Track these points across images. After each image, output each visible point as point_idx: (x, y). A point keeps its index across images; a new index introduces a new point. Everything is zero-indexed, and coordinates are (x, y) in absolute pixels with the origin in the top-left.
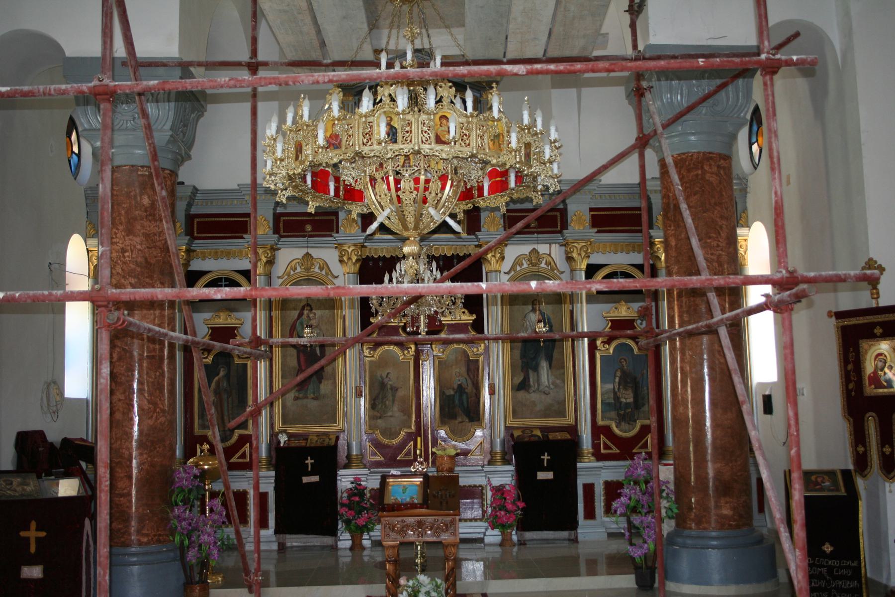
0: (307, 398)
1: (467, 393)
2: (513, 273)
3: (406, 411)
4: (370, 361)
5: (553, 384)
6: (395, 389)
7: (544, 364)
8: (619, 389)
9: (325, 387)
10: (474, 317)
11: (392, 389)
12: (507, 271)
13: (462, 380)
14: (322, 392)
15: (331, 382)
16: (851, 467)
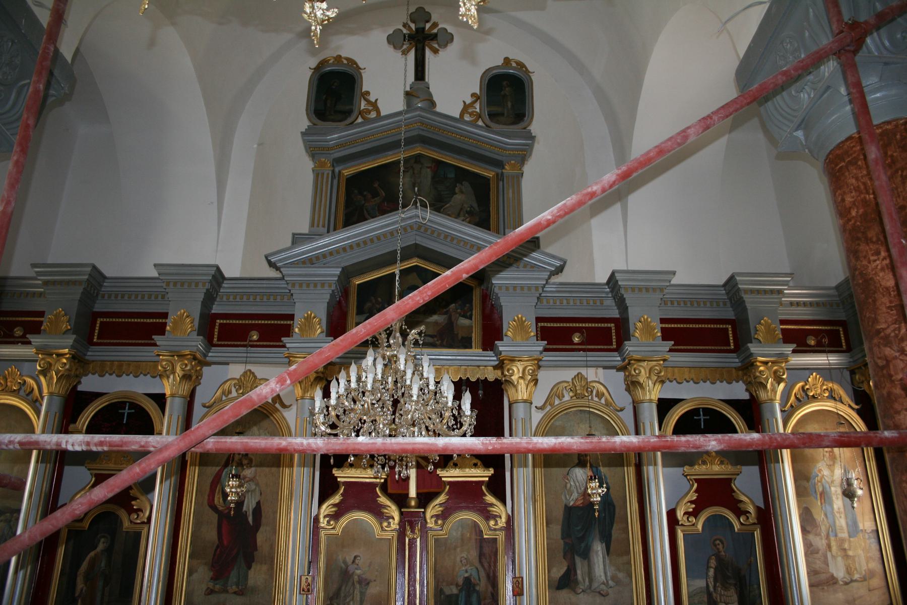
0: (227, 592)
1: (478, 592)
2: (548, 408)
5: (613, 578)
6: (365, 583)
7: (598, 548)
8: (715, 587)
9: (256, 576)
10: (491, 472)
11: (360, 582)
12: (540, 404)
13: (471, 572)
14: (251, 582)
15: (265, 568)
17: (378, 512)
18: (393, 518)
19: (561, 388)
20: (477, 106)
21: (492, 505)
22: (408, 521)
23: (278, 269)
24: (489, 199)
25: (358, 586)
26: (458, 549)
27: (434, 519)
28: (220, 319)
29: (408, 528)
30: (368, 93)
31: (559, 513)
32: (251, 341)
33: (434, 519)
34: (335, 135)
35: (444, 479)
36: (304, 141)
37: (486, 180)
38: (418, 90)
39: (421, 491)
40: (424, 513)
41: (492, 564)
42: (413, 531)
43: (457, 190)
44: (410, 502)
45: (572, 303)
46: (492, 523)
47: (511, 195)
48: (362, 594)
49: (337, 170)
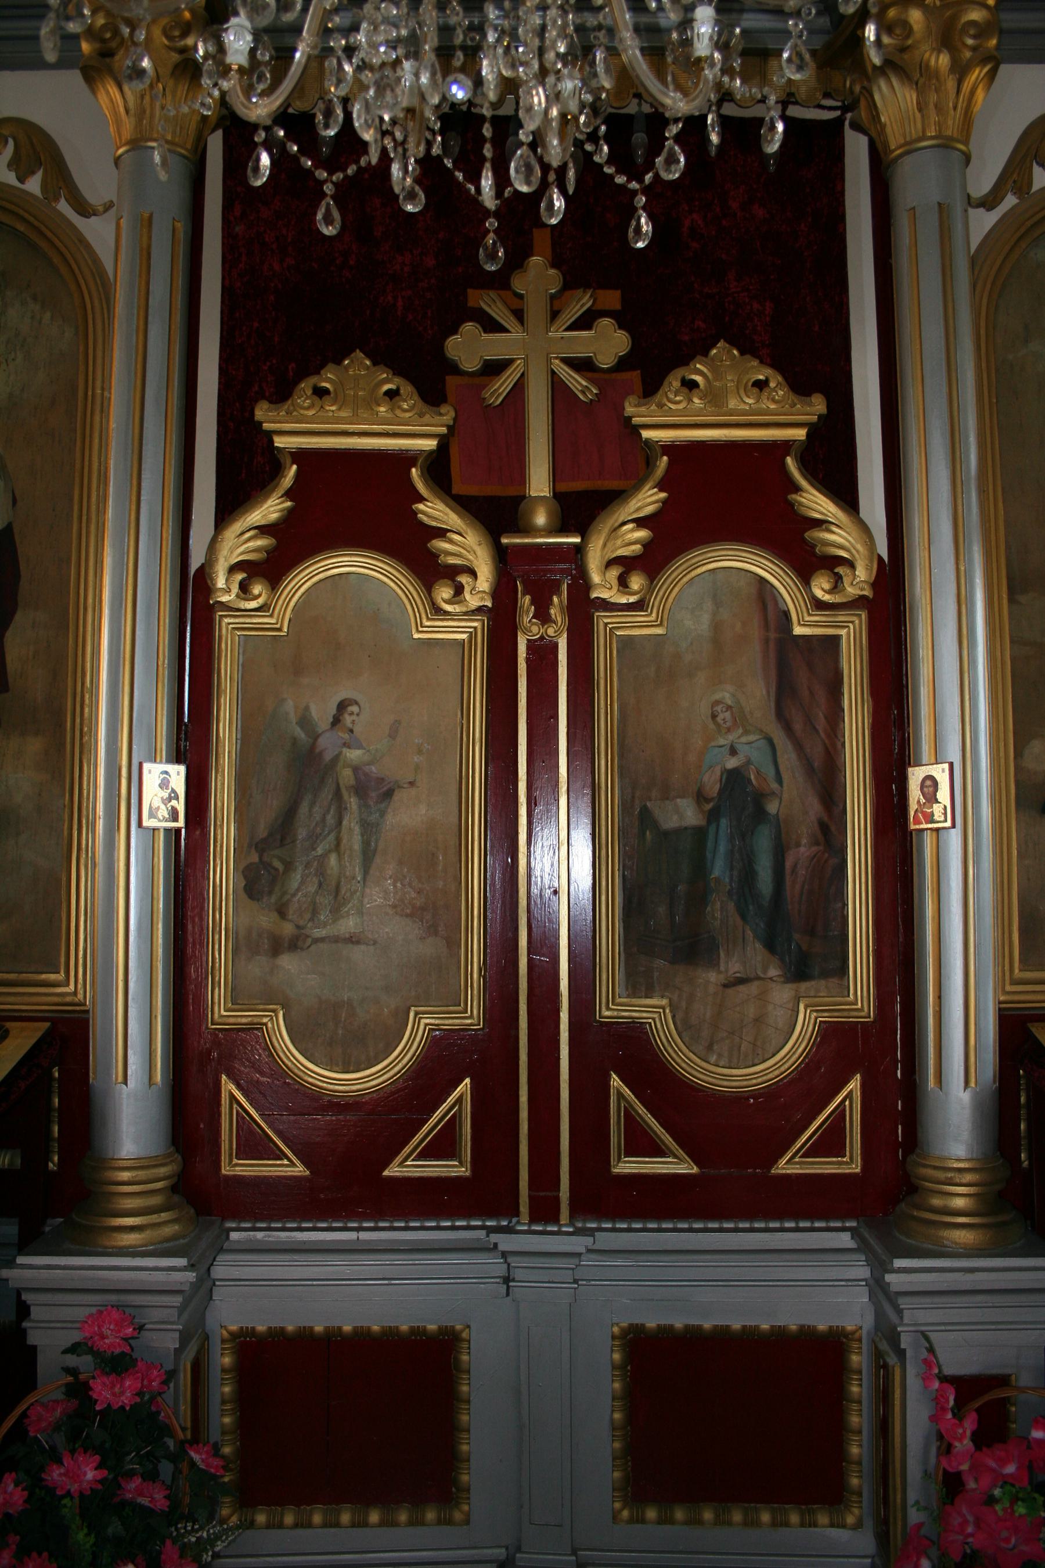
2: (1010, 201)
3: (438, 915)
6: (377, 792)
10: (818, 405)
13: (750, 751)
15: (34, 745)
17: (430, 571)
18: (473, 574)
27: (614, 573)
33: (614, 573)
35: (646, 434)
39: (563, 487)
40: (579, 551)
42: (543, 616)
44: (531, 512)
46: (821, 587)
48: (369, 829)
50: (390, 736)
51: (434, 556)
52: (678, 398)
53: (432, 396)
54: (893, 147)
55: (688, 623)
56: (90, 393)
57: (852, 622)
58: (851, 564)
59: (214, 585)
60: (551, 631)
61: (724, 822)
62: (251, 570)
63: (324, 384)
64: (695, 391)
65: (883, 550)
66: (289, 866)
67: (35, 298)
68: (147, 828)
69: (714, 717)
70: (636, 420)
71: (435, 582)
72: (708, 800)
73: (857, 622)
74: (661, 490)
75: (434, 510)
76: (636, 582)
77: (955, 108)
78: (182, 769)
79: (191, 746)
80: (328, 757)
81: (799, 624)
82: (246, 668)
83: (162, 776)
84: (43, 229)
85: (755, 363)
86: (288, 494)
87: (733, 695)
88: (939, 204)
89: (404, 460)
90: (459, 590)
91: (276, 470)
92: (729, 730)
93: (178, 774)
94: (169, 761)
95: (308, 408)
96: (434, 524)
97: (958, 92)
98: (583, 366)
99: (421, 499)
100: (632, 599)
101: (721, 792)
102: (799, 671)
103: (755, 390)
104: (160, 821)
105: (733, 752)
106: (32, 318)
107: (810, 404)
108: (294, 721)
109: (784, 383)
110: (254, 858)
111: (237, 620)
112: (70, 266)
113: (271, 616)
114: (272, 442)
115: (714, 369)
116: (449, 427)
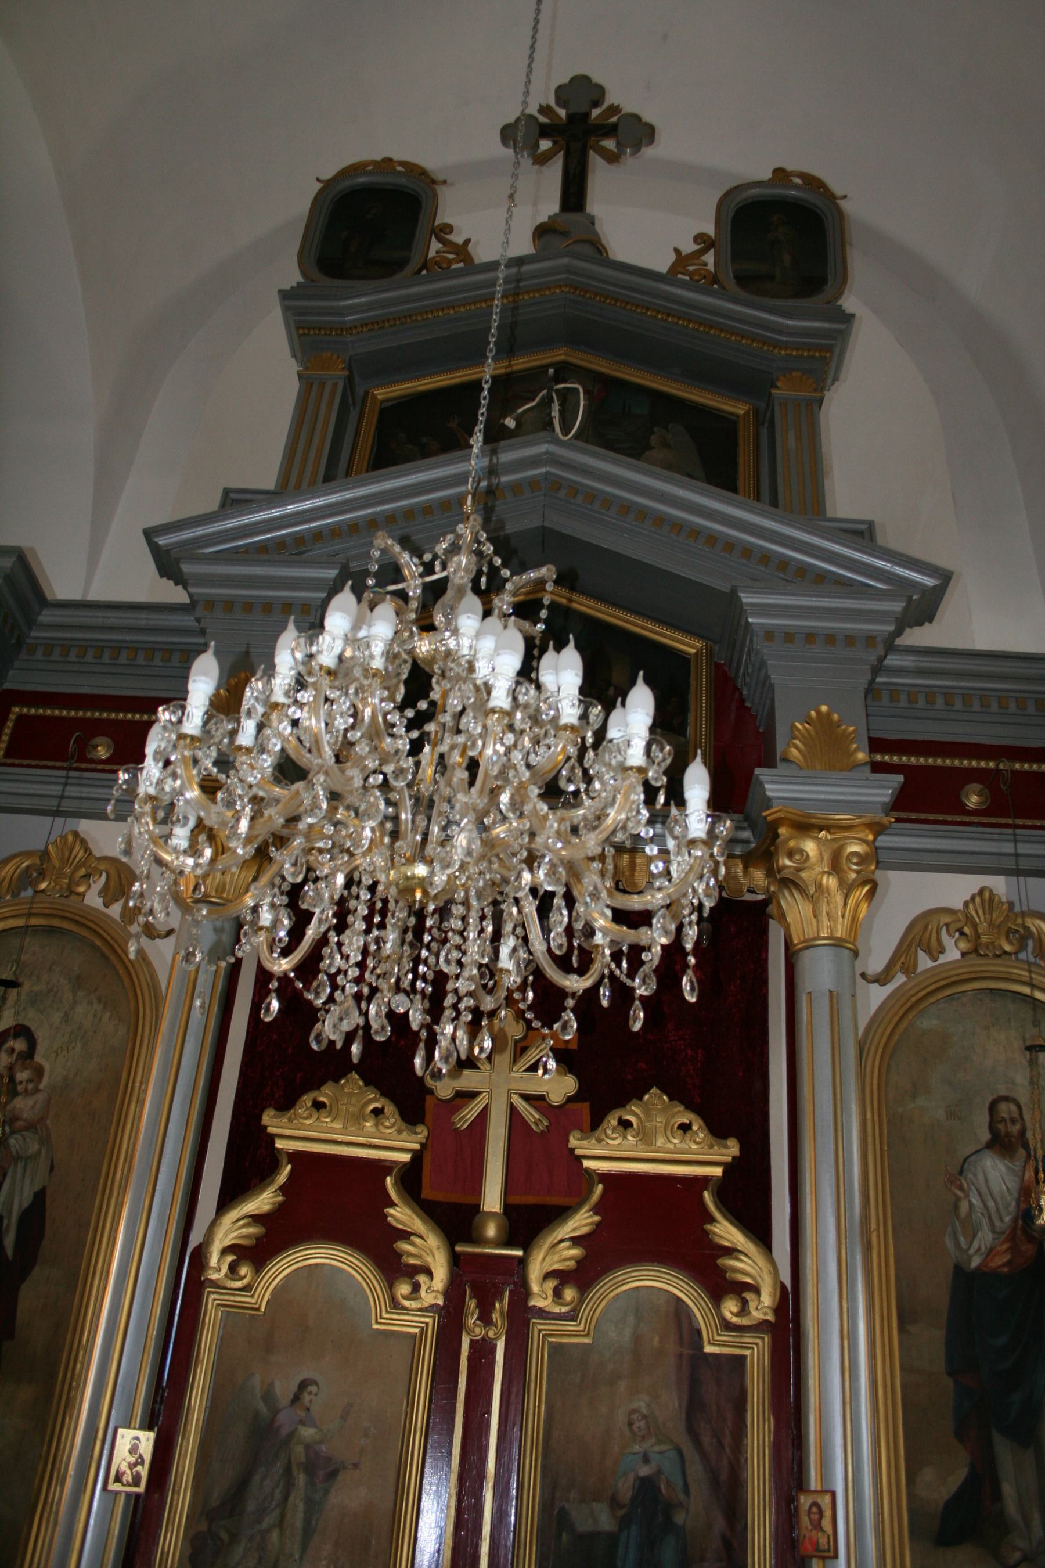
2: (900, 979)
4: (232, 1314)
6: (324, 1470)
10: (732, 1149)
16: (623, 112)
17: (393, 1267)
18: (430, 1274)
19: (932, 927)
20: (709, 258)
21: (731, 1251)
22: (479, 1280)
23: (180, 580)
24: (735, 464)
25: (301, 1479)
26: (622, 1385)
27: (551, 1284)
28: (23, 704)
29: (471, 1304)
30: (448, 228)
31: (937, 1291)
32: (92, 761)
33: (551, 1284)
34: (358, 301)
35: (586, 1164)
36: (286, 309)
37: (728, 425)
38: (570, 227)
39: (515, 1200)
40: (522, 1262)
41: (727, 1440)
42: (485, 1319)
43: (654, 440)
44: (483, 1226)
45: (958, 705)
46: (730, 1308)
47: (792, 442)
48: (312, 1506)
49: (360, 392)
50: (342, 1417)
51: (398, 1255)
52: (614, 1135)
53: (411, 1116)
54: (796, 942)
55: (613, 1335)
56: (130, 1085)
57: (757, 1344)
58: (756, 1290)
59: (208, 1263)
60: (491, 1334)
61: (634, 1529)
62: (239, 1252)
63: (322, 1099)
64: (629, 1130)
65: (786, 1279)
66: (234, 1538)
67: (99, 1000)
68: (111, 1491)
69: (630, 1424)
70: (578, 1152)
71: (397, 1278)
72: (621, 1506)
73: (761, 1344)
74: (596, 1214)
75: (401, 1214)
76: (569, 1294)
77: (843, 916)
78: (152, 1435)
79: (163, 1414)
80: (284, 1432)
81: (710, 1343)
82: (225, 1341)
83: (133, 1442)
84: (116, 946)
85: (681, 1108)
86: (283, 1189)
87: (648, 1406)
88: (830, 992)
89: (381, 1168)
90: (416, 1287)
91: (274, 1168)
92: (643, 1438)
93: (148, 1440)
94: (142, 1428)
95: (306, 1118)
96: (400, 1227)
97: (845, 905)
98: (535, 1100)
99: (392, 1204)
100: (564, 1309)
101: (634, 1499)
102: (708, 1388)
103: (680, 1132)
104: (123, 1485)
105: (646, 1460)
106: (95, 1015)
107: (726, 1147)
108: (259, 1395)
109: (704, 1127)
110: (204, 1526)
111: (222, 1297)
112: (132, 979)
113: (252, 1296)
114: (274, 1143)
115: (647, 1112)
116: (422, 1145)
